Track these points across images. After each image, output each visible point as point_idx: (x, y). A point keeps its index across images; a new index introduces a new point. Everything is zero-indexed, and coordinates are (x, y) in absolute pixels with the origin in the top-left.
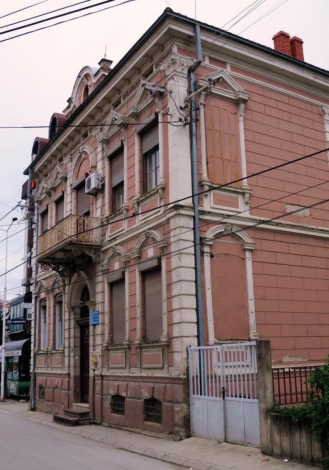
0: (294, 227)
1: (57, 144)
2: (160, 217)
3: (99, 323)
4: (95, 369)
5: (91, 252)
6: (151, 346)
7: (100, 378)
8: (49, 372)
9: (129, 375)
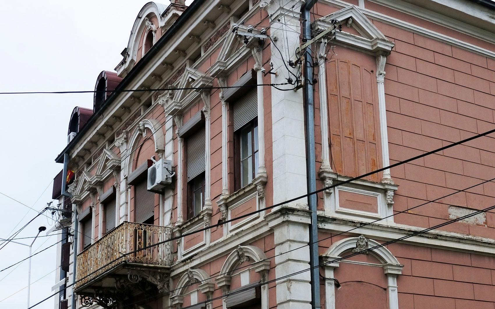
0: (461, 241)
2: (259, 227)
5: (156, 279)
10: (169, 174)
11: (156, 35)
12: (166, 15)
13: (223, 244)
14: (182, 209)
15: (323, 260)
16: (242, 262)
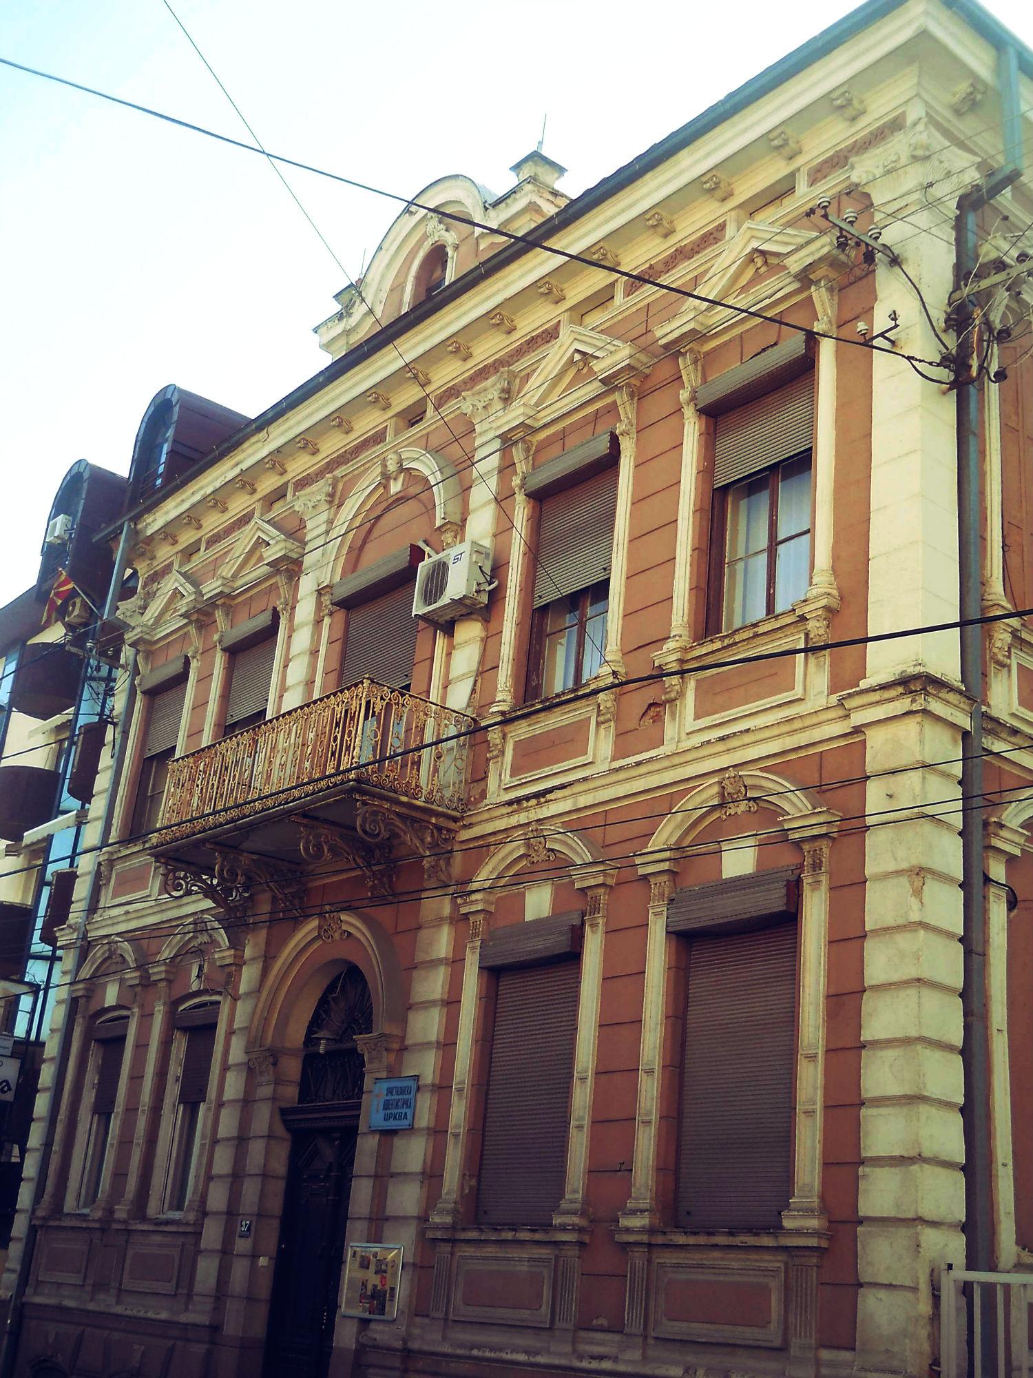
1: (272, 440)
2: (808, 722)
3: (416, 1126)
4: (370, 1321)
5: (422, 841)
6: (716, 1245)
7: (397, 1363)
8: (102, 1308)
9: (577, 1364)
10: (482, 580)
11: (455, 256)
12: (507, 205)
13: (666, 763)
14: (512, 671)
15: (990, 832)
16: (730, 814)
